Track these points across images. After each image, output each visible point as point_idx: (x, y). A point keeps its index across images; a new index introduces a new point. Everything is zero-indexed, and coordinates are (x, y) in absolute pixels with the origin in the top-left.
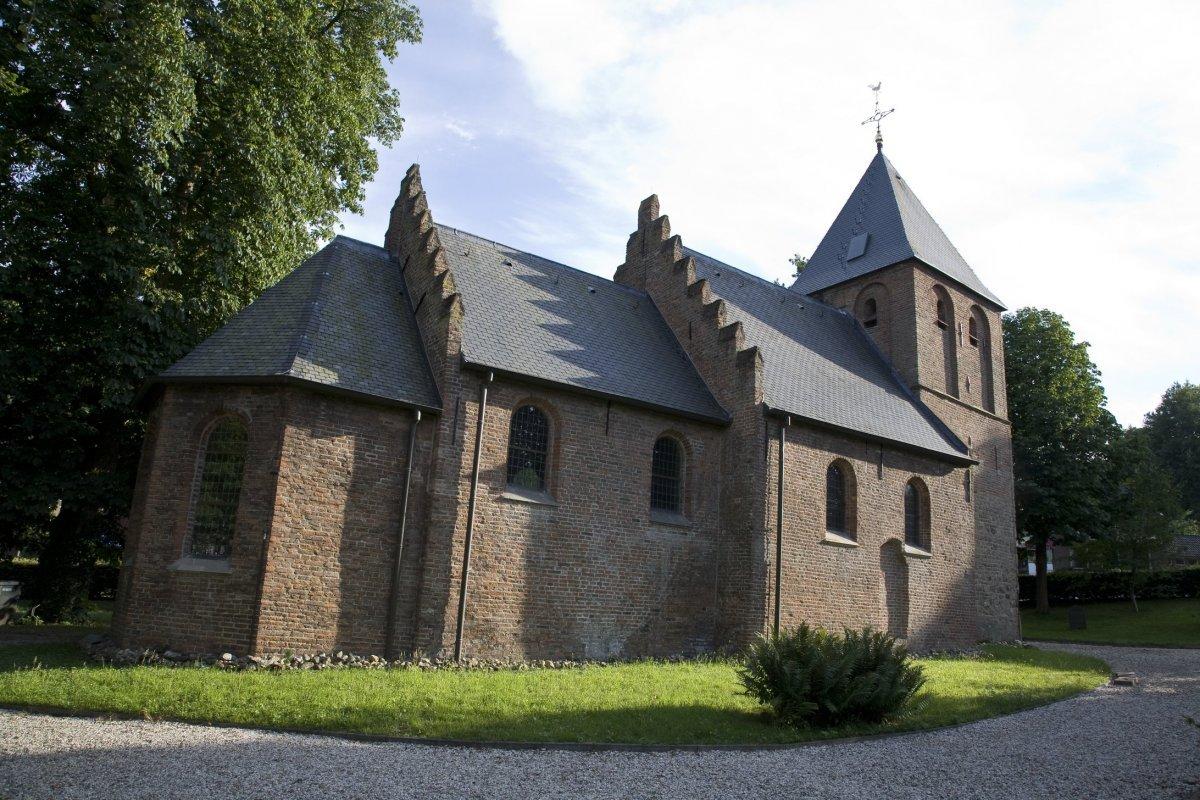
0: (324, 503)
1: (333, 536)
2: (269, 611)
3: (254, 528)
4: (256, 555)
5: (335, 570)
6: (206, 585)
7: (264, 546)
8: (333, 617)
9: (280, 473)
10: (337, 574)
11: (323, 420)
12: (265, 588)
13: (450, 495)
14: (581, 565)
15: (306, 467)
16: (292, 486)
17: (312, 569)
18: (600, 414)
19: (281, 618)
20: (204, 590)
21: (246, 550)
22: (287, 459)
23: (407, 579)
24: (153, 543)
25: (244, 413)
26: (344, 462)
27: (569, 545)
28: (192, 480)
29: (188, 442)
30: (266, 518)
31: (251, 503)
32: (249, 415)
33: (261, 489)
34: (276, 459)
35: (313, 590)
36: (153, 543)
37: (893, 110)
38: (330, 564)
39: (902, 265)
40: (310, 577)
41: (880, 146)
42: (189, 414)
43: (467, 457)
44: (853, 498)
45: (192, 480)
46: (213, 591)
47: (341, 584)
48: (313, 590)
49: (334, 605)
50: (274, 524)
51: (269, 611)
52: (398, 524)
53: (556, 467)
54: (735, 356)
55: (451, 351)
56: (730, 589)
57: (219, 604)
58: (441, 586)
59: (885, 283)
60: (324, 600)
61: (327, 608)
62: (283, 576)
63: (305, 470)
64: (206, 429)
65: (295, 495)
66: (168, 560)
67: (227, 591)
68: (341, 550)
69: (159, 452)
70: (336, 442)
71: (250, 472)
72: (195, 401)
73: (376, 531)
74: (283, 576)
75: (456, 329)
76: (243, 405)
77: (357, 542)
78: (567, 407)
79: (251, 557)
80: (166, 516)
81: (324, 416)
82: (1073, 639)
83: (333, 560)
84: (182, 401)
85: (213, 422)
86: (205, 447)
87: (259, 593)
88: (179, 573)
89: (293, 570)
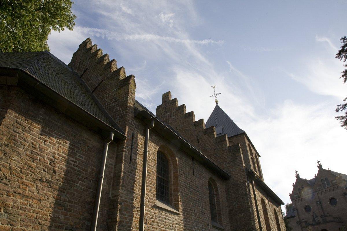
0: (27, 197)
13: (128, 200)
15: (16, 158)
26: (52, 162)
37: (220, 93)
39: (240, 135)
41: (217, 103)
52: (89, 224)
55: (130, 104)
70: (48, 143)
75: (132, 93)
81: (42, 119)
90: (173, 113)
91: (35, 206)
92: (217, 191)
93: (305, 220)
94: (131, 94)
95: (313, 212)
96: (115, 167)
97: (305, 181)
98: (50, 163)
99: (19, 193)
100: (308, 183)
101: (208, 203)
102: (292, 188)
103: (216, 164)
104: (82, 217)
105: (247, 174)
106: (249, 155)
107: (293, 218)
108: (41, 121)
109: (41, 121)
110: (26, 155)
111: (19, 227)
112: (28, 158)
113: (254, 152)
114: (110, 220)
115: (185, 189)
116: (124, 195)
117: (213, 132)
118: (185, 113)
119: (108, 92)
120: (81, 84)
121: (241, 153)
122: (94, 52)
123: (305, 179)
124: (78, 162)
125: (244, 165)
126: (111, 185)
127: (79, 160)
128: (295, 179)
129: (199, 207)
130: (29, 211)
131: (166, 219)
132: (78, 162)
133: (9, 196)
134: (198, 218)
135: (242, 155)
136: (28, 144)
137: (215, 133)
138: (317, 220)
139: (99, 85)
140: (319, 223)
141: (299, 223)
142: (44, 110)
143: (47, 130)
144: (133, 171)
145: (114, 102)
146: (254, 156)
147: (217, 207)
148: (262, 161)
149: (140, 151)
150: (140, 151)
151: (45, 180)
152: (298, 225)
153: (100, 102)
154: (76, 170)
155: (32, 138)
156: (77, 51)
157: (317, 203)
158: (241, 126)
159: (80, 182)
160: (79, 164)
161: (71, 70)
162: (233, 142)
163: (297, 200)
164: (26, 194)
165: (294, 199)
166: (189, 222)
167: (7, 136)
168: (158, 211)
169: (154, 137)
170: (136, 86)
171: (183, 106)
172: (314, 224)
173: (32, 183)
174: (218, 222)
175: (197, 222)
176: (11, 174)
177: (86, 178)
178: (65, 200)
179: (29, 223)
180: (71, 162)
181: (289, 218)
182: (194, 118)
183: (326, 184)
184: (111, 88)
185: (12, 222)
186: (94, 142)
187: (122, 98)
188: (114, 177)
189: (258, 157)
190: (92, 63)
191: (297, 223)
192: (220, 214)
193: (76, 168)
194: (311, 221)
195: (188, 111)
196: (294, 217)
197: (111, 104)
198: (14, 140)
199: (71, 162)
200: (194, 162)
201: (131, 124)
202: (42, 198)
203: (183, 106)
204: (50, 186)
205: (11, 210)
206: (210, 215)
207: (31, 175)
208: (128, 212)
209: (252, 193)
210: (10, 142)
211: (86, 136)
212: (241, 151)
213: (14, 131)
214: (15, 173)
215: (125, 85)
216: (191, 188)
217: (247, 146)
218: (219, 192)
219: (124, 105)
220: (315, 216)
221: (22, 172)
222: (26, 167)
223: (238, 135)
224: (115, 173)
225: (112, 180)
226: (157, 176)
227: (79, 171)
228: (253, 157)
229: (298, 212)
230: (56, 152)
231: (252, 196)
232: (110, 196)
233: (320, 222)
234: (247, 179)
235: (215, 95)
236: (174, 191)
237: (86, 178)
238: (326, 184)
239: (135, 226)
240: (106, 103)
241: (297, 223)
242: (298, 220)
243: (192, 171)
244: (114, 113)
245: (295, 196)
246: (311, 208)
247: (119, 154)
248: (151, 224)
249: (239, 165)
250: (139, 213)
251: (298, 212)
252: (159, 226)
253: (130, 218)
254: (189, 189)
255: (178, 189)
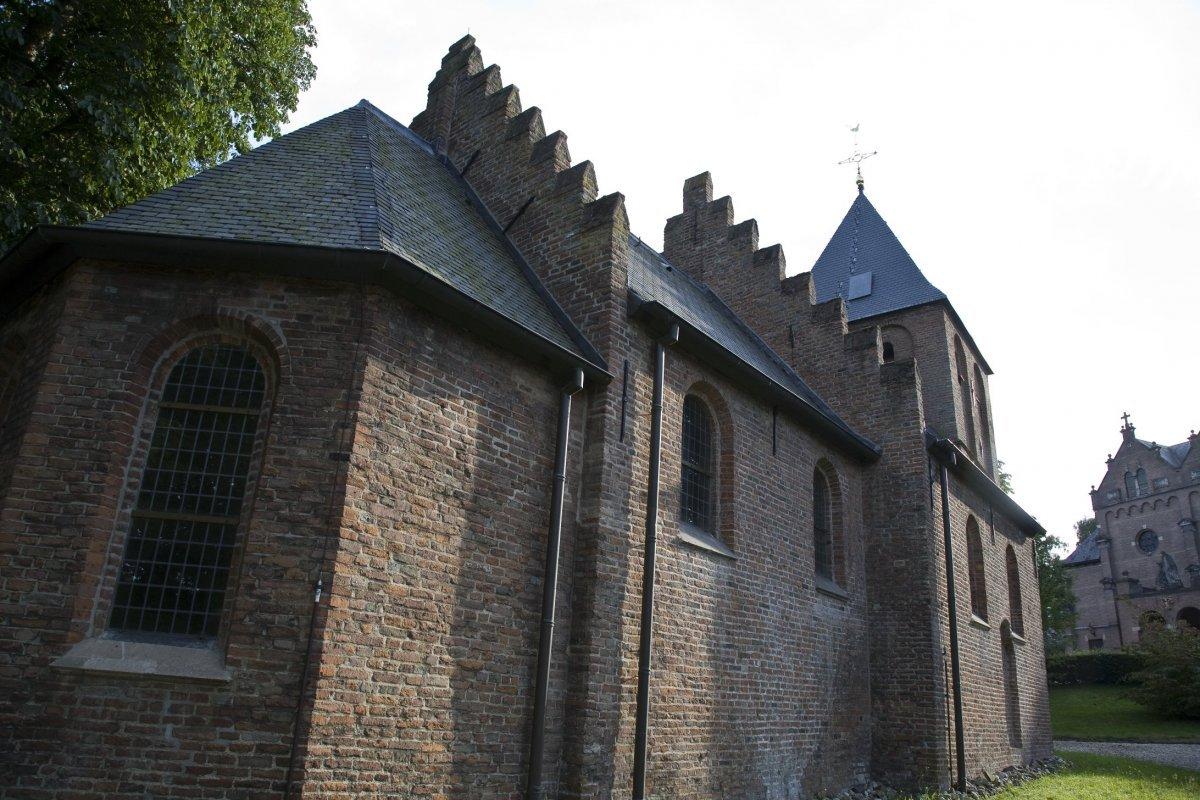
0: (426, 529)
1: (440, 597)
2: (322, 770)
3: (288, 575)
4: (294, 637)
5: (441, 672)
6: (159, 707)
7: (315, 618)
8: (437, 773)
9: (353, 458)
10: (445, 680)
11: (427, 361)
12: (317, 717)
13: (619, 530)
14: (759, 657)
15: (398, 450)
16: (374, 490)
17: (404, 669)
18: (767, 423)
19: (346, 783)
20: (154, 720)
21: (266, 625)
22: (366, 431)
23: (552, 691)
24: (14, 601)
25: (268, 326)
26: (461, 450)
27: (749, 623)
28: (125, 463)
29: (123, 377)
30: (316, 554)
31: (281, 519)
32: (279, 331)
33: (303, 489)
34: (344, 426)
35: (404, 715)
36: (14, 601)
38: (434, 657)
40: (401, 686)
41: (861, 188)
42: (130, 319)
43: (638, 465)
44: (979, 567)
45: (125, 463)
46: (176, 721)
47: (455, 699)
48: (404, 715)
49: (440, 748)
50: (338, 568)
51: (322, 770)
52: (539, 581)
53: (728, 496)
54: (877, 370)
55: (616, 284)
56: (896, 688)
57: (193, 753)
58: (609, 696)
59: (906, 326)
60: (423, 737)
61: (428, 753)
62: (352, 687)
63: (398, 458)
64: (166, 354)
65: (378, 509)
66: (57, 644)
67: (217, 723)
68: (455, 628)
69: (48, 393)
70: (448, 409)
71: (282, 452)
72: (146, 294)
73: (506, 593)
74: (352, 687)
76: (266, 311)
77: (478, 612)
78: (737, 406)
79: (279, 643)
80: (56, 539)
82: (1118, 736)
83: (439, 652)
84: (114, 290)
85: (183, 342)
86: (161, 393)
87: (301, 729)
88: (83, 676)
89: (370, 672)
90: (718, 246)
91: (440, 546)
92: (837, 495)
93: (1133, 576)
94: (618, 252)
95: (1163, 553)
96: (586, 449)
97: (1154, 448)
98: (457, 453)
99: (412, 523)
100: (1163, 456)
101: (810, 529)
102: (1104, 469)
103: (841, 415)
104: (524, 567)
105: (928, 450)
106: (954, 371)
107: (1092, 567)
108: (431, 358)
109: (431, 358)
110: (413, 441)
111: (421, 588)
112: (418, 448)
113: (971, 360)
114: (580, 575)
115: (749, 495)
116: (611, 519)
117: (838, 316)
118: (754, 250)
119: (551, 238)
120: (469, 202)
121: (919, 386)
122: (493, 96)
123: (1154, 443)
124: (508, 445)
125: (923, 424)
126: (579, 495)
127: (511, 441)
128: (1119, 440)
129: (786, 540)
130: (433, 558)
131: (701, 571)
132: (508, 445)
133: (398, 529)
134: (780, 567)
135: (919, 394)
136: (413, 417)
137: (845, 321)
138: (1172, 578)
139: (522, 210)
140: (1178, 588)
141: (1111, 583)
142: (432, 331)
143: (443, 379)
144: (627, 458)
145: (572, 271)
146: (969, 375)
147: (835, 538)
148: (996, 388)
149: (642, 407)
150: (642, 407)
151: (451, 493)
152: (1105, 589)
153: (530, 266)
154: (506, 465)
155: (419, 402)
156: (439, 67)
157: (1183, 524)
158: (937, 271)
159: (516, 491)
160: (512, 450)
161: (431, 152)
162: (904, 328)
163: (1115, 510)
164: (424, 524)
165: (1105, 507)
166: (757, 578)
167: (376, 404)
168: (683, 554)
169: (676, 364)
170: (628, 224)
171: (750, 227)
172: (1159, 588)
173: (430, 501)
174: (833, 578)
175: (778, 578)
176: (394, 485)
177: (528, 482)
178: (492, 532)
179: (435, 582)
180: (495, 447)
181: (1078, 565)
182: (782, 267)
183: (1137, 487)
184: (560, 228)
185: (409, 579)
186: (538, 394)
187: (593, 262)
188: (584, 475)
189: (983, 374)
190: (493, 134)
191: (1104, 582)
192: (840, 559)
193: (506, 460)
194: (1149, 580)
195: (764, 242)
196: (1097, 562)
197: (562, 275)
198: (389, 411)
199: (495, 447)
200: (777, 418)
201: (622, 338)
202: (451, 531)
203: (750, 227)
204: (462, 504)
205: (404, 557)
206: (811, 562)
207: (427, 484)
208: (620, 557)
209: (938, 503)
210: (384, 418)
211: (520, 379)
212: (918, 381)
213: (387, 391)
214: (400, 482)
215: (601, 224)
216: (766, 491)
217: (950, 341)
218: (843, 497)
219: (600, 282)
220: (1167, 565)
221: (411, 480)
222: (417, 468)
223: (926, 304)
224: (586, 466)
225: (581, 482)
226: (684, 466)
227: (512, 467)
228: (966, 378)
229: (1110, 550)
230: (466, 428)
231: (939, 512)
232: (578, 519)
233: (1182, 586)
234: (927, 466)
235: (858, 158)
236: (722, 502)
237: (528, 482)
238: (1137, 487)
239: (633, 587)
240: (550, 271)
241: (1104, 582)
242: (1108, 573)
243: (771, 446)
244: (573, 303)
245: (1110, 496)
246: (1160, 538)
247: (596, 416)
248: (668, 584)
249: (906, 424)
250: (642, 559)
251: (1110, 550)
252: (685, 587)
253: (622, 569)
254: (760, 494)
255: (732, 495)
